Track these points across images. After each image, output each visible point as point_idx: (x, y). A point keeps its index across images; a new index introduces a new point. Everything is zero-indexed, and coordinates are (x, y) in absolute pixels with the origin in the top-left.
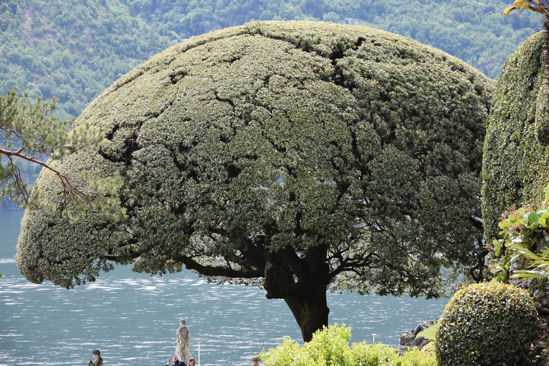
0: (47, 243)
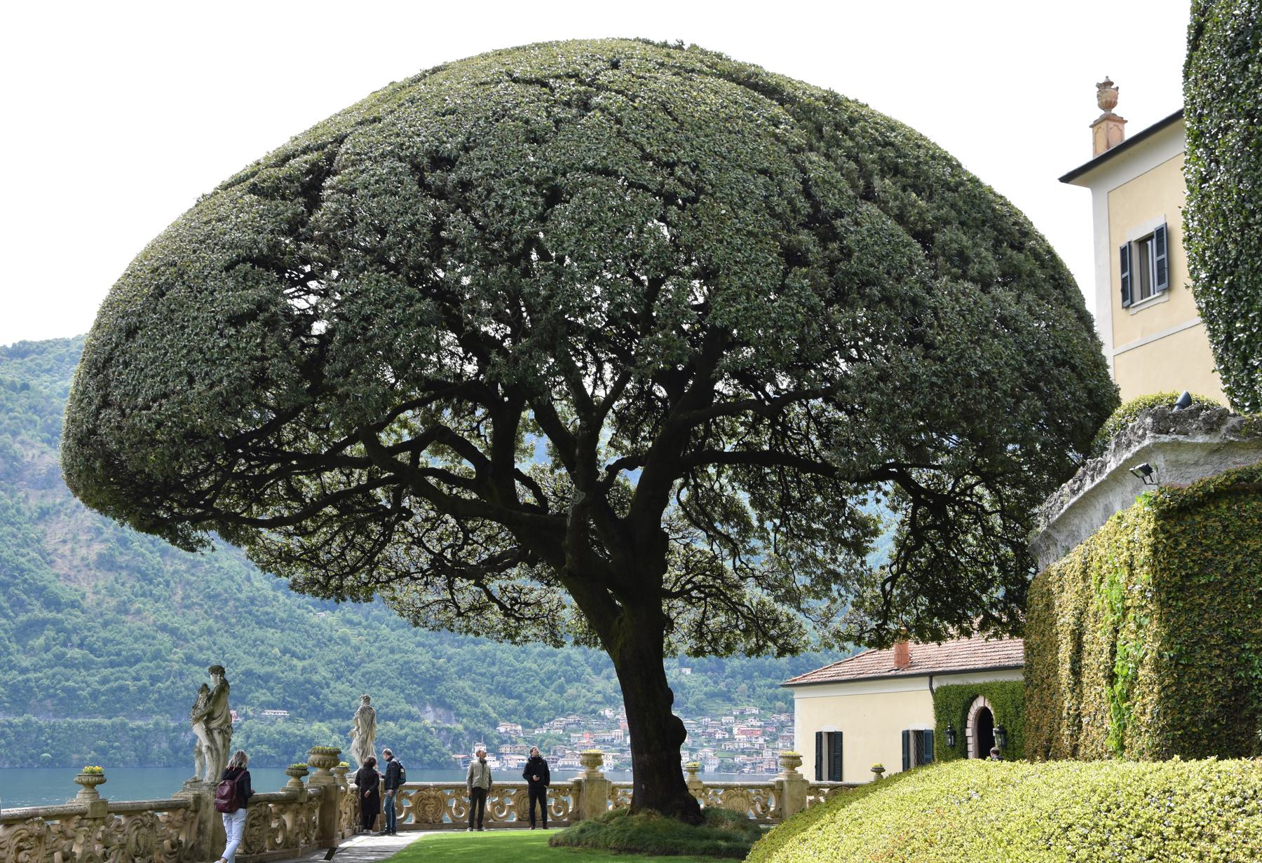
0: (120, 374)
